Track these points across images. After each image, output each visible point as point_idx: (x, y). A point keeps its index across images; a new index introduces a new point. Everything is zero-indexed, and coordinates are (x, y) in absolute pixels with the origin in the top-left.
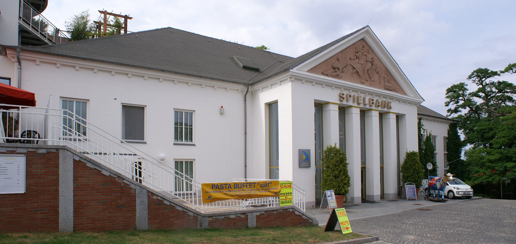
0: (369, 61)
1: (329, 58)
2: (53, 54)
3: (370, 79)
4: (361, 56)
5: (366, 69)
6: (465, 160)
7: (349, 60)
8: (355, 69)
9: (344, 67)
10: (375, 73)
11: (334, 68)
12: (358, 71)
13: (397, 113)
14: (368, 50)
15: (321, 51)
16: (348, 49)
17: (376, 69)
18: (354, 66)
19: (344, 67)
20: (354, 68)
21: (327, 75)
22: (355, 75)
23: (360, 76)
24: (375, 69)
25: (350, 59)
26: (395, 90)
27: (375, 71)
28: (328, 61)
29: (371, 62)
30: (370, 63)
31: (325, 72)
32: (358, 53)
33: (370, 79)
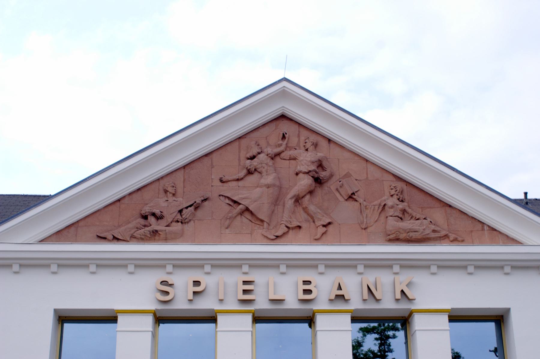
0: (300, 172)
1: (130, 194)
2: (456, 171)
3: (314, 222)
4: (264, 165)
5: (289, 196)
6: (397, 324)
7: (221, 184)
8: (240, 204)
9: (187, 208)
10: (343, 200)
11: (145, 217)
12: (250, 208)
13: (452, 309)
14: (306, 143)
15: (12, 228)
16: (214, 155)
17: (340, 190)
18: (235, 199)
19: (187, 208)
20: (235, 202)
21: (116, 239)
22: (245, 219)
23: (262, 221)
24: (337, 190)
25: (221, 181)
26: (446, 236)
27: (341, 194)
28: (126, 201)
29: (308, 173)
30: (306, 176)
31: (108, 231)
32: (255, 159)
33: (314, 222)
